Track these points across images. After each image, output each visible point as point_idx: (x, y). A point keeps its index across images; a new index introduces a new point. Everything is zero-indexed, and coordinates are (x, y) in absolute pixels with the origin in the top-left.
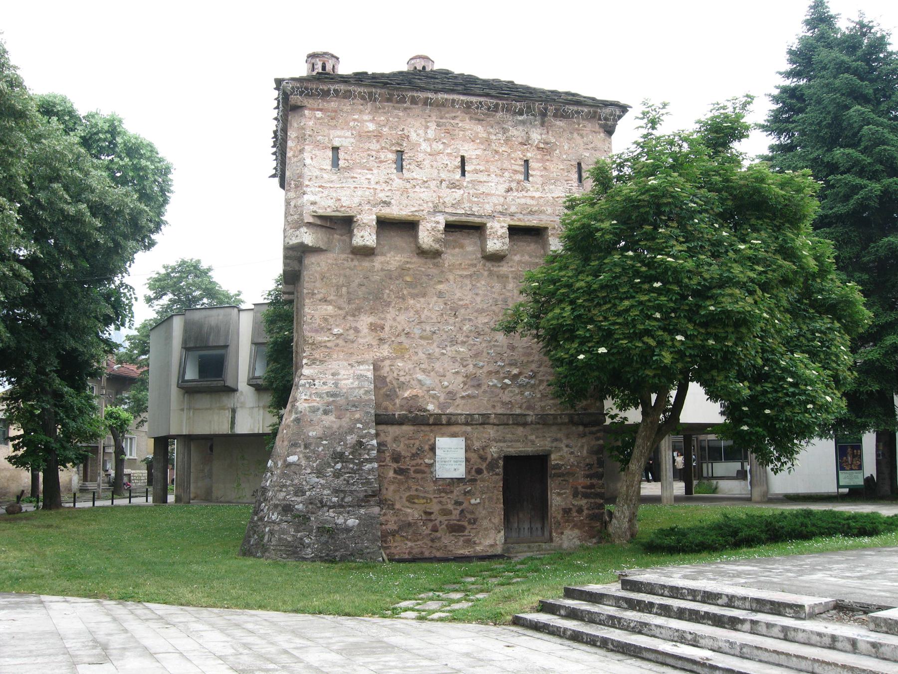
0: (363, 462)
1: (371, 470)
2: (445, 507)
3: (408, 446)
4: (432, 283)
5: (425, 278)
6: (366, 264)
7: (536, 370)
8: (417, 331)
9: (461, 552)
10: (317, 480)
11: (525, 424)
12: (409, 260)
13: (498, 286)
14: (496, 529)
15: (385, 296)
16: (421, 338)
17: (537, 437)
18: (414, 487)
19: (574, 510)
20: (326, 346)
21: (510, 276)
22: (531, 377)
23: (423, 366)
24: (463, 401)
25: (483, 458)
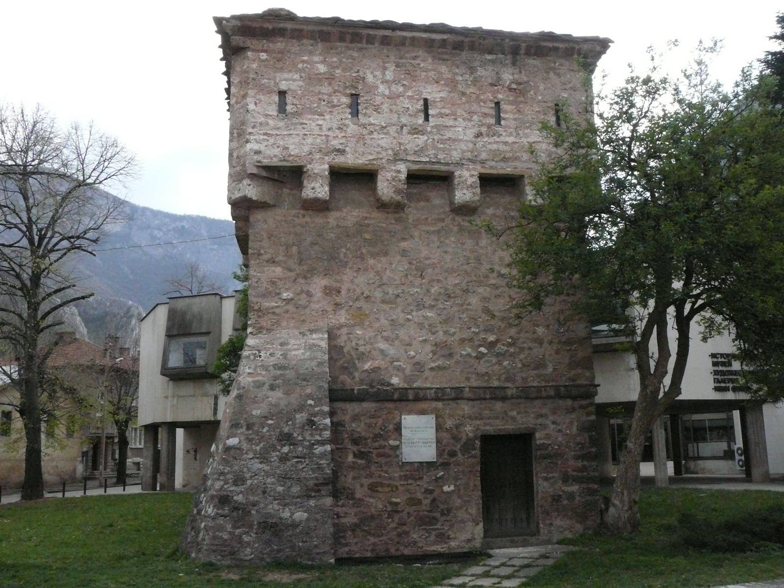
0: (313, 444)
1: (323, 455)
6: (319, 220)
7: (516, 336)
8: (378, 294)
9: (433, 548)
10: (260, 466)
11: (504, 399)
12: (368, 215)
13: (469, 243)
14: (474, 521)
15: (342, 256)
16: (383, 302)
17: (518, 413)
20: (274, 313)
22: (510, 345)
23: (385, 334)
25: (456, 438)
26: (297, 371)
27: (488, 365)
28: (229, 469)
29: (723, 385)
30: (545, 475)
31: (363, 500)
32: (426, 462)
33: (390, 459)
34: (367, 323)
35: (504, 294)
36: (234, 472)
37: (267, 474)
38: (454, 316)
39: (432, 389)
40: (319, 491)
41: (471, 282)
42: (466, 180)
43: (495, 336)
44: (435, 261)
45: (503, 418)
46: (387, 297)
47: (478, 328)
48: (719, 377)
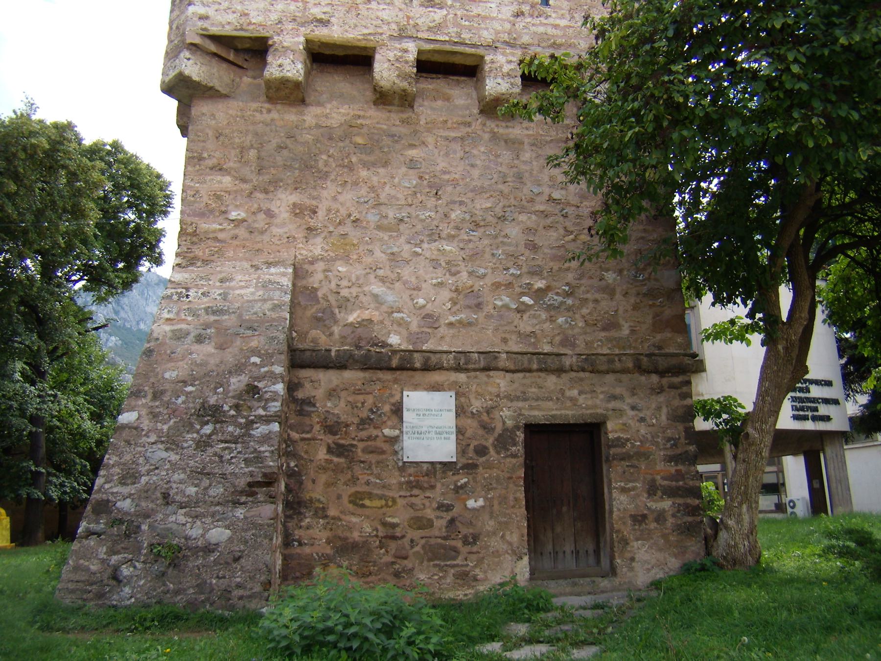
0: (253, 422)
1: (266, 439)
2: (419, 514)
3: (353, 406)
4: (398, 147)
5: (386, 141)
6: (290, 116)
7: (575, 283)
8: (372, 218)
9: (451, 595)
10: (164, 455)
11: (560, 371)
12: (361, 113)
13: (506, 156)
14: (514, 552)
15: (321, 164)
16: (379, 228)
17: (581, 393)
18: (363, 478)
19: (651, 517)
20: (216, 239)
21: (526, 141)
22: (568, 295)
23: (380, 273)
24: (451, 331)
25: (486, 428)
26: (240, 316)
27: (535, 321)
28: (117, 459)
29: (801, 413)
30: (622, 484)
31: (340, 520)
32: (440, 463)
33: (384, 457)
34: (355, 257)
35: (556, 225)
36: (124, 464)
37: (174, 467)
38: (484, 252)
39: (451, 352)
40: (253, 494)
41: (510, 206)
42: (501, 67)
43: (544, 282)
44: (457, 176)
45: (558, 399)
46: (385, 222)
47: (520, 269)
48: (798, 405)
